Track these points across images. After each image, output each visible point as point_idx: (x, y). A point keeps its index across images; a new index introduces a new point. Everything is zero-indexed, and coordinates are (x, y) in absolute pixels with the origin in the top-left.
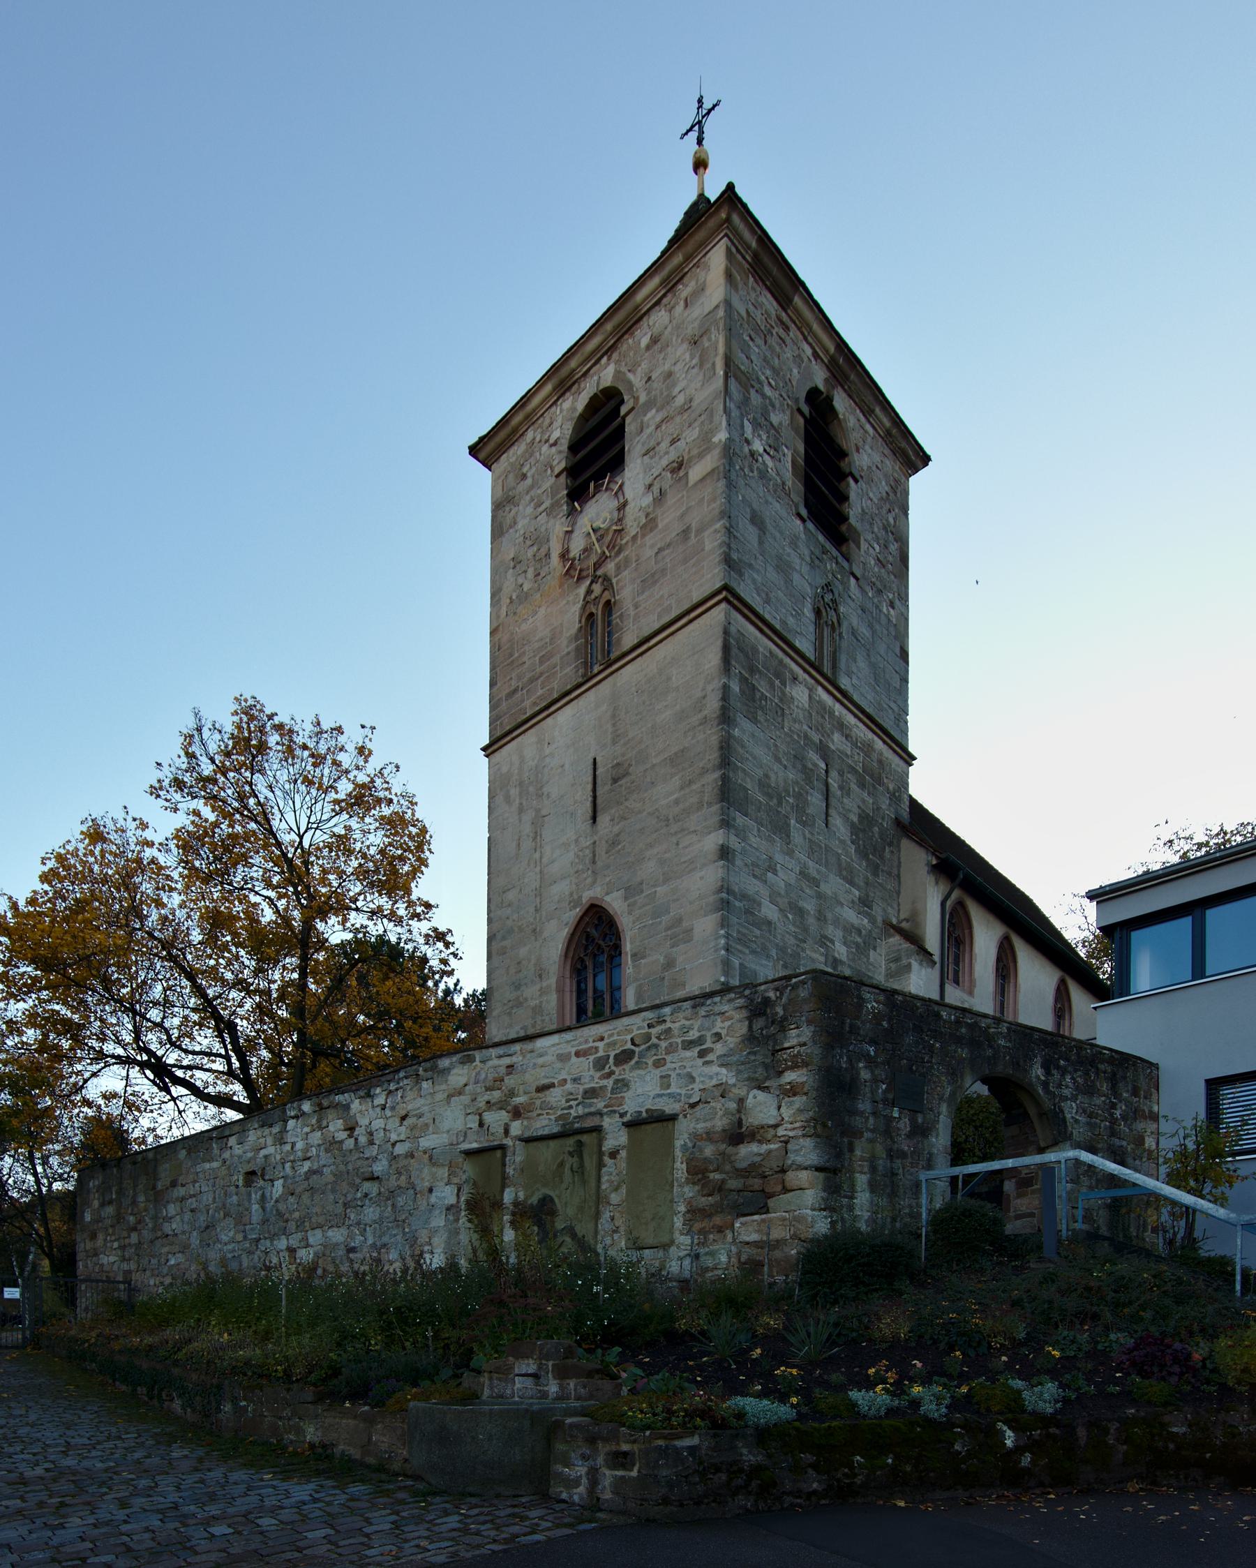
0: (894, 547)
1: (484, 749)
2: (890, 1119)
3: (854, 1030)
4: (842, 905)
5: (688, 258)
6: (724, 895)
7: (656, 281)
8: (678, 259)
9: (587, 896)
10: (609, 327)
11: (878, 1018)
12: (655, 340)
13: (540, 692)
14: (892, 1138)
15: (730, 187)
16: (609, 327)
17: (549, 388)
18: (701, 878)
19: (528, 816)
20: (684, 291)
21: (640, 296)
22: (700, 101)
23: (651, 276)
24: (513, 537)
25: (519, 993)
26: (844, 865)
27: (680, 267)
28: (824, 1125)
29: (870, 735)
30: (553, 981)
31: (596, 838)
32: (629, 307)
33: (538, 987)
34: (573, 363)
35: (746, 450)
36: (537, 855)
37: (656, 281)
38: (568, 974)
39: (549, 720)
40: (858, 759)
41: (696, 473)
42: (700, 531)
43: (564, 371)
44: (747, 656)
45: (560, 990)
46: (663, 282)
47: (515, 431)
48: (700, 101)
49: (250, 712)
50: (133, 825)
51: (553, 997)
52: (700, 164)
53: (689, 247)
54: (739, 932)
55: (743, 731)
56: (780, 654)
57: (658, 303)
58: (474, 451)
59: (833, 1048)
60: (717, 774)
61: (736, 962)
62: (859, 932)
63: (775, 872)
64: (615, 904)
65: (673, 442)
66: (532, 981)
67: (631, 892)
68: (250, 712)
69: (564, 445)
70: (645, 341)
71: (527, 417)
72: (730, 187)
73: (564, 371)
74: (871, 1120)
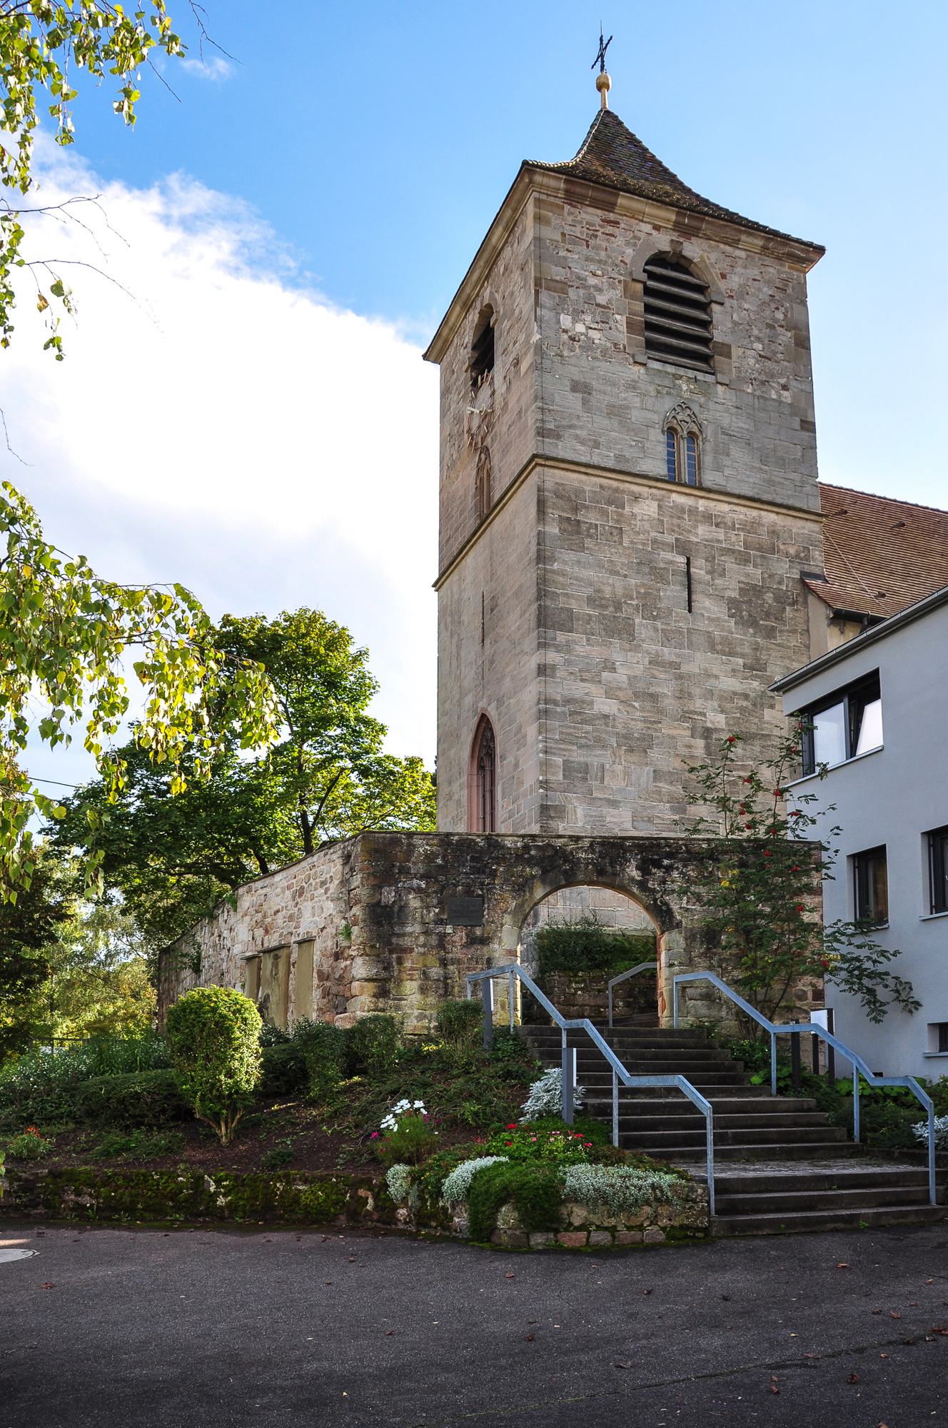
0: (786, 337)
2: (442, 936)
3: (405, 871)
4: (716, 677)
5: (515, 211)
6: (542, 706)
7: (500, 229)
8: (509, 213)
10: (481, 263)
11: (430, 858)
12: (506, 269)
14: (445, 949)
16: (481, 263)
17: (458, 308)
19: (454, 640)
20: (518, 231)
21: (494, 240)
22: (601, 40)
24: (450, 416)
26: (718, 640)
27: (512, 217)
28: (373, 947)
29: (755, 513)
32: (489, 249)
34: (468, 290)
35: (565, 337)
37: (500, 229)
40: (737, 541)
41: (524, 366)
42: (526, 411)
44: (569, 499)
45: (470, 787)
46: (505, 229)
47: (446, 341)
48: (601, 40)
52: (602, 86)
53: (513, 204)
54: (561, 733)
55: (565, 563)
56: (615, 484)
57: (506, 242)
59: (381, 887)
60: (535, 606)
61: (559, 760)
62: (746, 696)
63: (614, 670)
64: (493, 714)
69: (470, 346)
70: (502, 269)
71: (451, 329)
73: (464, 297)
74: (422, 939)
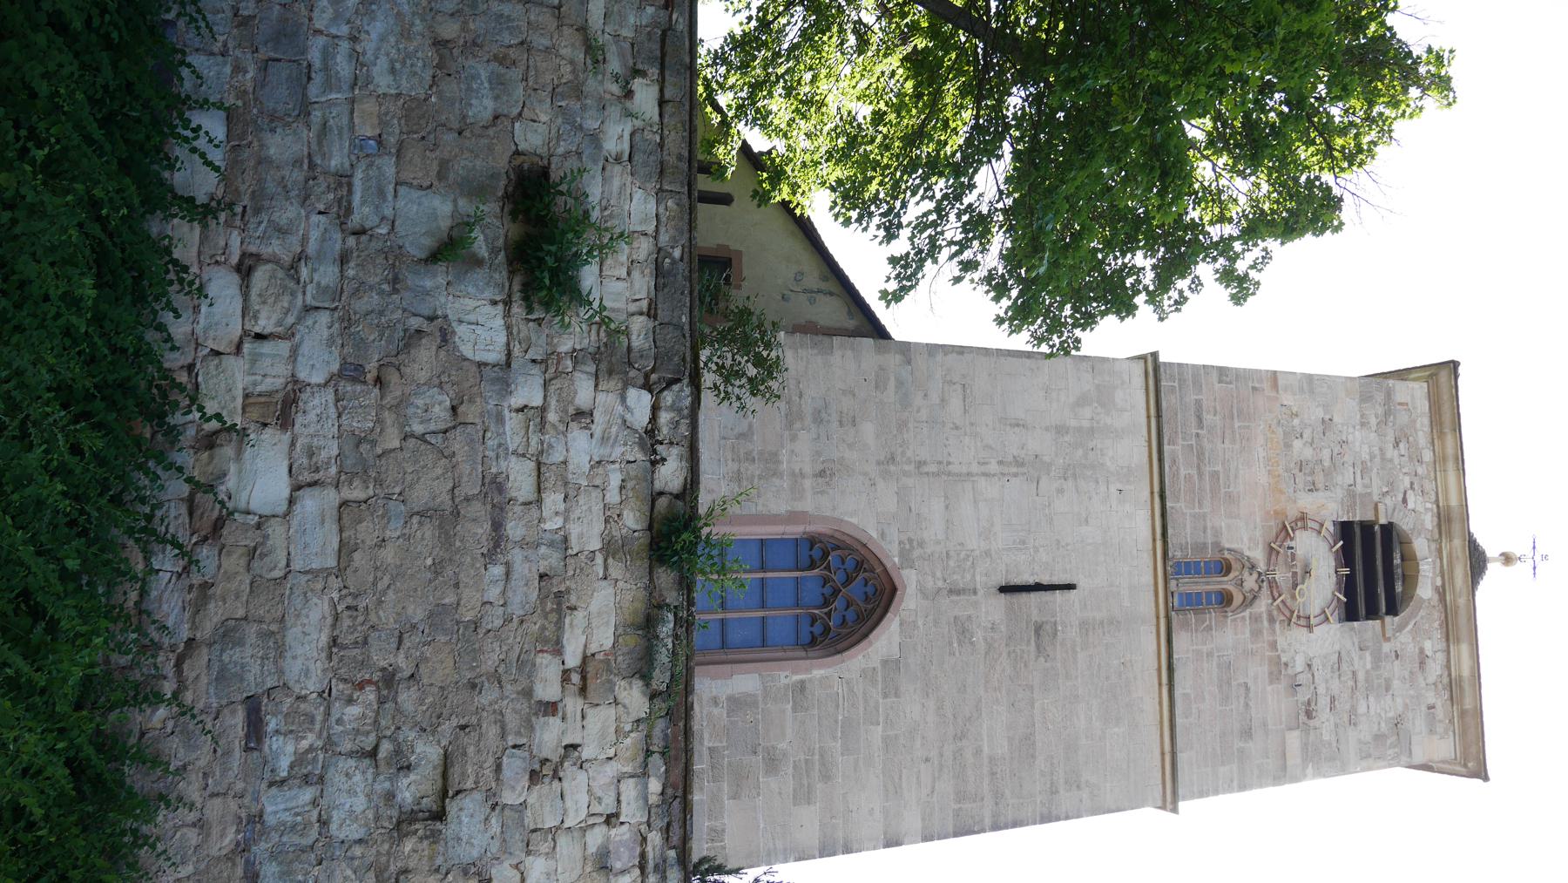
1: (1155, 355)
9: (910, 581)
13: (1183, 472)
15: (1486, 778)
18: (871, 811)
23: (1472, 668)
25: (808, 420)
30: (807, 505)
31: (981, 593)
33: (808, 469)
36: (993, 467)
38: (813, 528)
39: (1147, 493)
43: (1451, 465)
45: (794, 517)
49: (1175, 810)
50: (148, 510)
51: (780, 506)
58: (1442, 378)
65: (1333, 700)
66: (818, 453)
67: (892, 666)
68: (1175, 810)
72: (1486, 778)
